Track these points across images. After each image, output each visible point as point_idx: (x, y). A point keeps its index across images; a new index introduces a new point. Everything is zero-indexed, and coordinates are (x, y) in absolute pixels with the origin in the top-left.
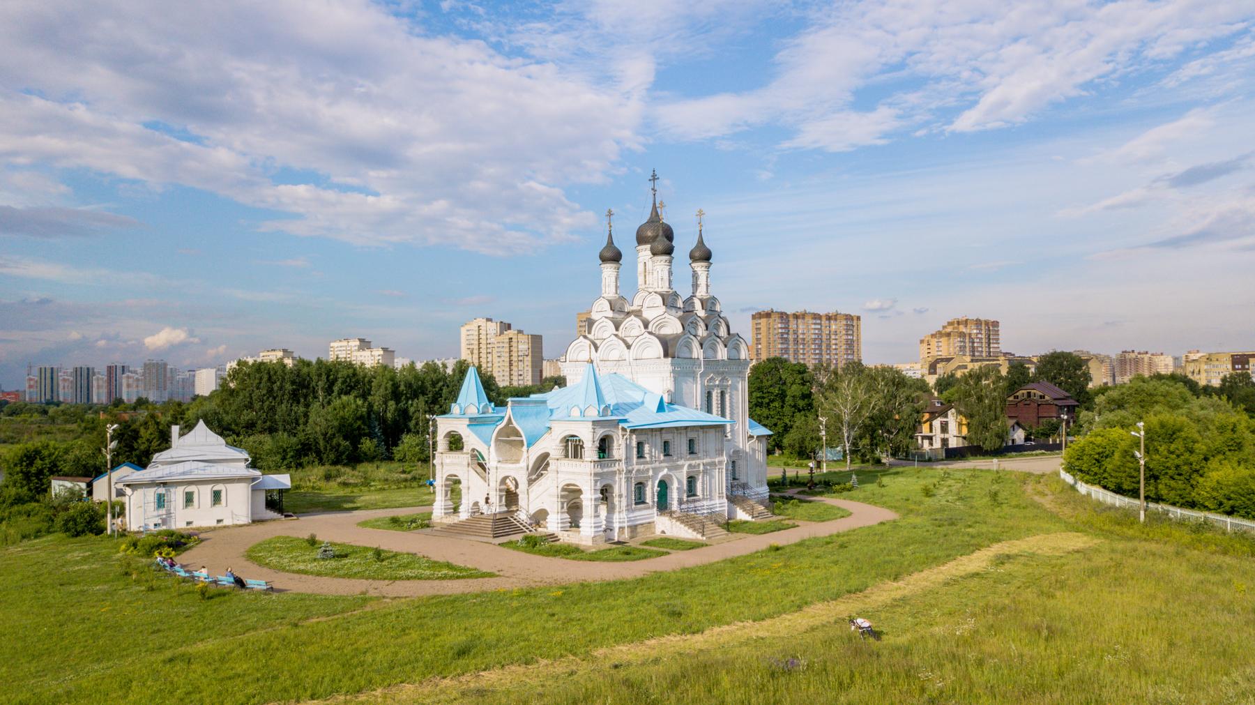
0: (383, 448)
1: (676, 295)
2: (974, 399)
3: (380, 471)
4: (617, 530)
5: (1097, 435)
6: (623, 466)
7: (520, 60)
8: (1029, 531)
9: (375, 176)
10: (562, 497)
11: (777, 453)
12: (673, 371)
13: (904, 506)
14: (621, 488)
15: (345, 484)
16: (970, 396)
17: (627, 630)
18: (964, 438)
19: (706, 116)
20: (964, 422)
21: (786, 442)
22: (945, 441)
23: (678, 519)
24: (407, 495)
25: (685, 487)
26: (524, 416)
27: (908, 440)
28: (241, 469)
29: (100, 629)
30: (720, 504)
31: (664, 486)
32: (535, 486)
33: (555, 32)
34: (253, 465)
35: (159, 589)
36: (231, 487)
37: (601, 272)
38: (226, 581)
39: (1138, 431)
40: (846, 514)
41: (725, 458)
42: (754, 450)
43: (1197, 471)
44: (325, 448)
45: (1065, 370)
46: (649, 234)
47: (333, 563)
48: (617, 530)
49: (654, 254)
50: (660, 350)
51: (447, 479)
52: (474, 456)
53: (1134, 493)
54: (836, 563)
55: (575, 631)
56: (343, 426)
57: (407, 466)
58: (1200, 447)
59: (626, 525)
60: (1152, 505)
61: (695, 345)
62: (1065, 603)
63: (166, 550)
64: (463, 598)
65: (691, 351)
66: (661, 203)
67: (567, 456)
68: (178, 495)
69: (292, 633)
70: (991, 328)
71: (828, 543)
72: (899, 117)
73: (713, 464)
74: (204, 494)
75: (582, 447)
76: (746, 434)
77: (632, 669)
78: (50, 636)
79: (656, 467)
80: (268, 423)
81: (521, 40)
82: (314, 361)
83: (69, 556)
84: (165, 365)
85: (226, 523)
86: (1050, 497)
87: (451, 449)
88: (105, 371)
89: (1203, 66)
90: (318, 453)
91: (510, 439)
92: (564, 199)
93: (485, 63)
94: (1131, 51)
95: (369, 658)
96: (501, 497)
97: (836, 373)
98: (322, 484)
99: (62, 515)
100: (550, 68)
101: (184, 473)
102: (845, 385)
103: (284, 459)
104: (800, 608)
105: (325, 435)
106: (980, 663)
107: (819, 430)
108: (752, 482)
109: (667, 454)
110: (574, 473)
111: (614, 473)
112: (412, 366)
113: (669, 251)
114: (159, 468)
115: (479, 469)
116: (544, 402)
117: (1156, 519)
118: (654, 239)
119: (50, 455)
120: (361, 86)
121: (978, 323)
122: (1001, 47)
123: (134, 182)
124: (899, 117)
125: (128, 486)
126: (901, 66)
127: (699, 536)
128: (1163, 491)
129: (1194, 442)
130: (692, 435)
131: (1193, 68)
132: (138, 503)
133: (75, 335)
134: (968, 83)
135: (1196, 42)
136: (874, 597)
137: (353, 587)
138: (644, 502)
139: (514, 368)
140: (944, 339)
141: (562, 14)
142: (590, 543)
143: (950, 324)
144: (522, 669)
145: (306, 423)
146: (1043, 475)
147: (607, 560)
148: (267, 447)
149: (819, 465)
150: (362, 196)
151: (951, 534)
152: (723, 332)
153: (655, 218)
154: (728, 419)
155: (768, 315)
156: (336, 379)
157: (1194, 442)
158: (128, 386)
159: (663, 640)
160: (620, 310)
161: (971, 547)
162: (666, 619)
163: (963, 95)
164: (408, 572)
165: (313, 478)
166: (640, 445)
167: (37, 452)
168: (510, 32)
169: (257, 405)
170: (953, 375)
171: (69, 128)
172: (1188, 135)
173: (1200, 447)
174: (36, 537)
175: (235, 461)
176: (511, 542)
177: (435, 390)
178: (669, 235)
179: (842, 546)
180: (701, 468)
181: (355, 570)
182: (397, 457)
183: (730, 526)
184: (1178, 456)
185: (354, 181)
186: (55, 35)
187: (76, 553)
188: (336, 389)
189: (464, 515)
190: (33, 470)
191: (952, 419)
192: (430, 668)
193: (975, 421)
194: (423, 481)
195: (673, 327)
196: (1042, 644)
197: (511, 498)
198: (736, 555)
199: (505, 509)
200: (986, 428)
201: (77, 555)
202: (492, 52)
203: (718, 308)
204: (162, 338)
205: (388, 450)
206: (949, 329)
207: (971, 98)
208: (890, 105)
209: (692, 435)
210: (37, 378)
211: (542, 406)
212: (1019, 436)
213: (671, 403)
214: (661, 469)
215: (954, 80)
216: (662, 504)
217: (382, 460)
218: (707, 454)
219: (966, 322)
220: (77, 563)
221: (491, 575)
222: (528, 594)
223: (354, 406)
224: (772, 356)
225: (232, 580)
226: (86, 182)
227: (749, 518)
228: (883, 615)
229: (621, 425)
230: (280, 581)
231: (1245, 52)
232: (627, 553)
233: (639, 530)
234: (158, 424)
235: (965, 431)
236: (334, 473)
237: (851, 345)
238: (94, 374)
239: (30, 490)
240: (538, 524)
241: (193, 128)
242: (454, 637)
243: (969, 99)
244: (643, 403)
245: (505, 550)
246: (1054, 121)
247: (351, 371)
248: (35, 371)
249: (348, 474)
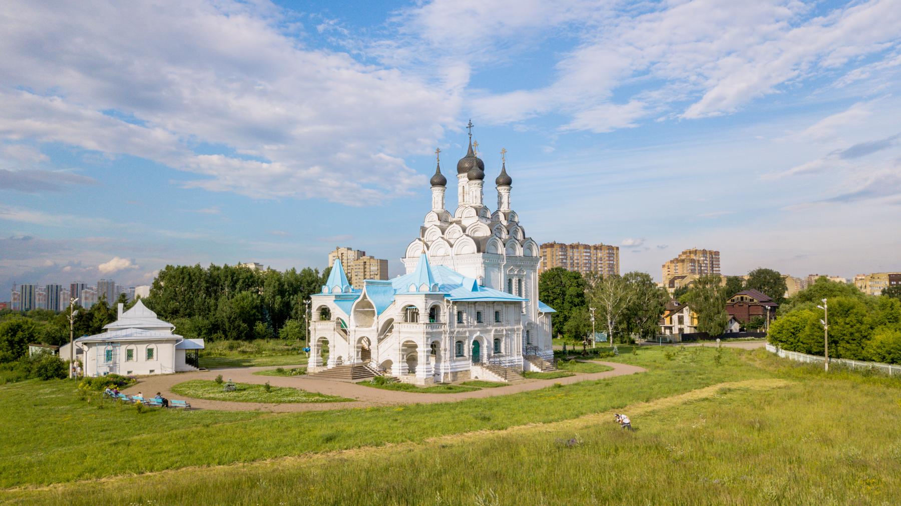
0: (271, 330)
1: (486, 208)
2: (702, 299)
3: (271, 344)
4: (442, 375)
5: (792, 316)
6: (447, 328)
7: (373, 67)
8: (744, 378)
9: (268, 149)
10: (403, 350)
11: (559, 337)
12: (484, 263)
13: (654, 365)
14: (445, 344)
15: (244, 352)
16: (700, 296)
17: (451, 427)
18: (695, 328)
19: (505, 107)
20: (695, 316)
21: (565, 328)
22: (681, 330)
23: (488, 368)
25: (493, 346)
26: (375, 293)
27: (655, 326)
28: (168, 334)
29: (63, 429)
30: (518, 359)
31: (477, 344)
32: (383, 343)
33: (399, 47)
34: (177, 332)
35: (107, 408)
36: (160, 346)
37: (432, 193)
38: (155, 401)
39: (823, 304)
41: (522, 327)
42: (543, 323)
43: (865, 337)
44: (230, 328)
45: (768, 282)
46: (467, 165)
47: (235, 394)
48: (442, 375)
49: (470, 179)
51: (319, 341)
52: (338, 323)
53: (821, 354)
54: (604, 393)
55: (412, 428)
56: (243, 312)
57: (288, 342)
58: (867, 319)
59: (449, 371)
60: (833, 360)
61: (500, 244)
62: (771, 413)
63: (112, 386)
64: (331, 412)
65: (497, 249)
67: (406, 321)
68: (121, 351)
69: (204, 430)
70: (713, 257)
71: (597, 384)
72: (646, 108)
73: (513, 330)
74: (140, 351)
75: (418, 314)
76: (537, 312)
77: (454, 449)
78: (27, 432)
79: (471, 331)
80: (188, 311)
81: (373, 53)
82: (222, 267)
83: (41, 391)
84: (113, 283)
85: (156, 372)
86: (758, 362)
87: (322, 319)
89: (862, 73)
90: (224, 332)
91: (365, 310)
92: (404, 166)
93: (348, 69)
94: (812, 62)
95: (261, 442)
96: (358, 352)
97: (601, 278)
98: (227, 352)
99: (35, 367)
100: (395, 73)
101: (126, 336)
104: (577, 416)
105: (229, 318)
106: (711, 442)
108: (541, 346)
109: (479, 321)
110: (411, 333)
111: (441, 333)
112: (294, 270)
113: (481, 177)
114: (112, 332)
115: (342, 333)
116: (390, 284)
117: (834, 369)
118: (470, 168)
119: (29, 328)
120: (260, 85)
121: (704, 252)
122: (718, 59)
123: (94, 152)
124: (646, 108)
125: (85, 344)
126: (646, 72)
127: (503, 380)
128: (842, 352)
129: (864, 316)
130: (498, 308)
131: (855, 74)
132: (90, 359)
133: (49, 263)
134: (694, 84)
135: (857, 56)
136: (632, 411)
137: (252, 407)
138: (462, 356)
140: (679, 264)
141: (404, 34)
142: (423, 383)
143: (684, 253)
144: (374, 448)
145: (216, 309)
146: (753, 350)
148: (186, 327)
149: (590, 342)
150: (259, 163)
151: (685, 379)
152: (520, 236)
153: (471, 155)
154: (524, 297)
155: (552, 246)
156: (238, 280)
157: (864, 316)
158: (86, 298)
159: (477, 433)
160: (444, 219)
162: (479, 422)
163: (692, 92)
164: (290, 398)
165: (220, 348)
166: (460, 314)
167: (19, 326)
168: (366, 47)
169: (180, 298)
171: (49, 114)
172: (853, 122)
173: (867, 319)
174: (17, 381)
175: (165, 329)
176: (365, 382)
178: (481, 166)
179: (607, 385)
180: (504, 332)
181: (251, 397)
182: (282, 336)
183: (525, 374)
184: (852, 327)
185: (253, 152)
186: (40, 48)
187: (47, 390)
188: (238, 286)
189: (331, 365)
190: (16, 339)
191: (686, 314)
192: (307, 447)
193: (703, 315)
195: (484, 231)
196: (756, 434)
197: (365, 354)
200: (711, 319)
201: (48, 390)
202: (353, 61)
203: (516, 220)
204: (112, 265)
205: (275, 331)
206: (683, 257)
207: (697, 95)
208: (640, 99)
209: (498, 308)
210: (19, 293)
211: (388, 288)
212: (735, 327)
213: (481, 286)
214: (475, 332)
215: (685, 82)
216: (476, 358)
217: (271, 338)
218: (508, 323)
219: (695, 252)
220: (47, 394)
221: (350, 400)
222: (378, 410)
223: (250, 299)
224: (555, 267)
225: (160, 401)
226: (60, 153)
227: (539, 370)
228: (638, 421)
229: (446, 298)
230: (194, 404)
231: (892, 63)
232: (450, 388)
233: (459, 375)
234: (108, 309)
235: (696, 322)
236: (236, 345)
237: (611, 267)
238: (61, 290)
239: (13, 353)
240: (385, 371)
241: (138, 114)
242: (324, 430)
243: (696, 96)
244: (462, 285)
245: (361, 387)
246: (757, 111)
247: (249, 274)
248: (19, 288)
249: (246, 346)
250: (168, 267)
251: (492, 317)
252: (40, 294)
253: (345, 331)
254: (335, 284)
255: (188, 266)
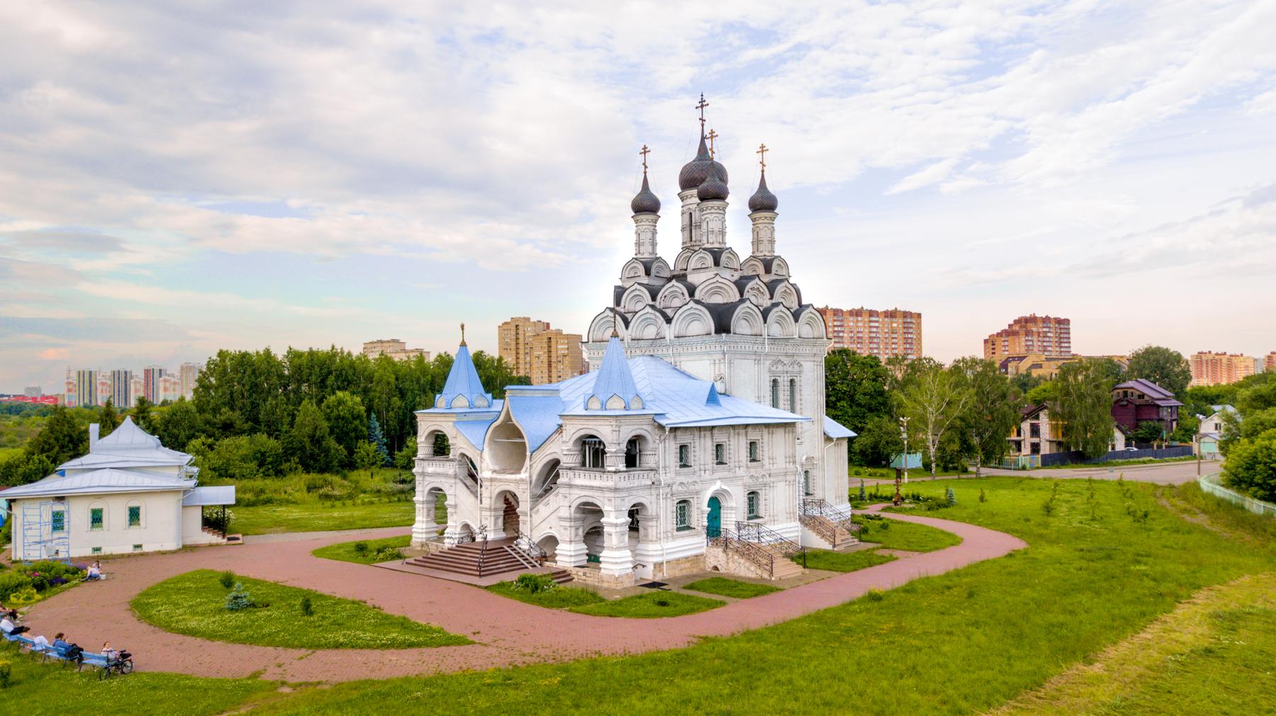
0: (384, 454)
14: (661, 511)
24: (386, 511)
40: (955, 541)
50: (710, 325)
56: (308, 425)
66: (712, 132)
75: (604, 453)
85: (146, 549)
88: (142, 375)
102: (929, 379)
103: (260, 465)
107: (899, 434)
108: (830, 499)
110: (592, 488)
115: (469, 482)
139: (554, 370)
145: (292, 424)
147: (637, 616)
148: (243, 452)
161: (1164, 597)
170: (1029, 375)
175: (172, 466)
177: (426, 381)
178: (720, 173)
194: (406, 491)
198: (822, 607)
199: (503, 535)
210: (76, 382)
232: (663, 604)
238: (132, 377)
248: (74, 375)
250: (221, 354)
251: (744, 453)
252: (103, 384)
253: (473, 477)
254: (462, 390)
255: (251, 350)
